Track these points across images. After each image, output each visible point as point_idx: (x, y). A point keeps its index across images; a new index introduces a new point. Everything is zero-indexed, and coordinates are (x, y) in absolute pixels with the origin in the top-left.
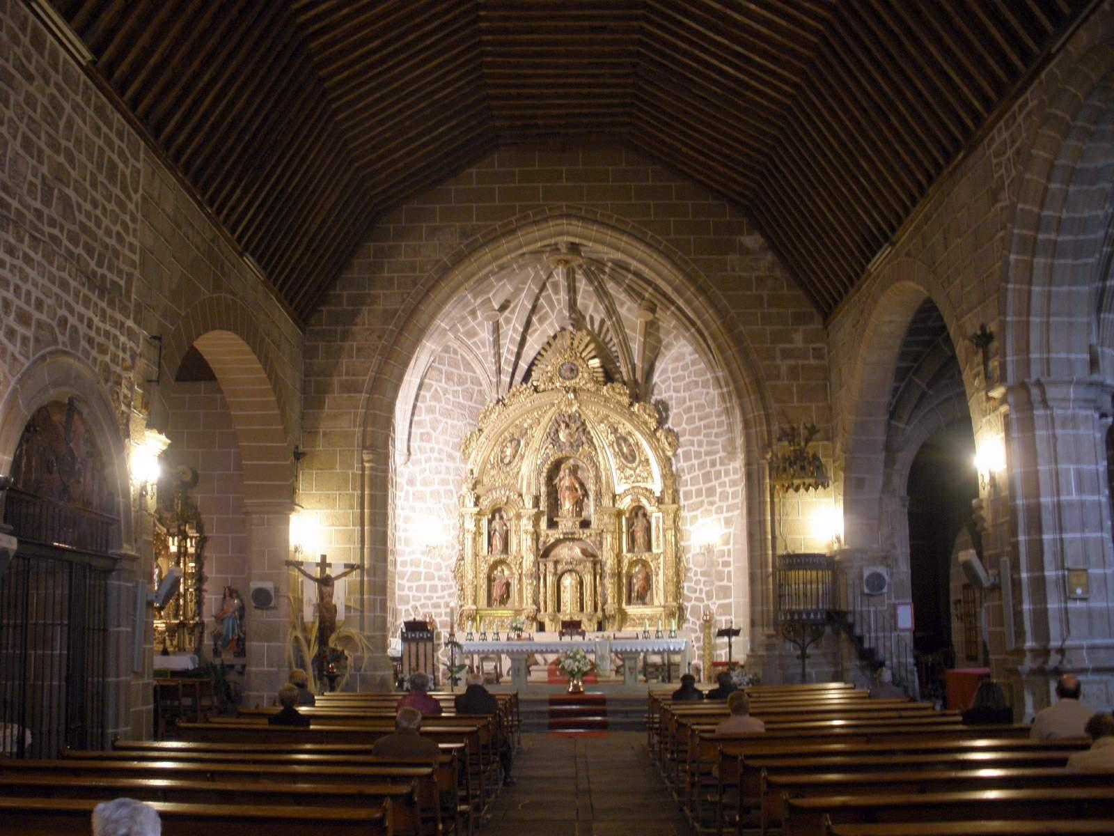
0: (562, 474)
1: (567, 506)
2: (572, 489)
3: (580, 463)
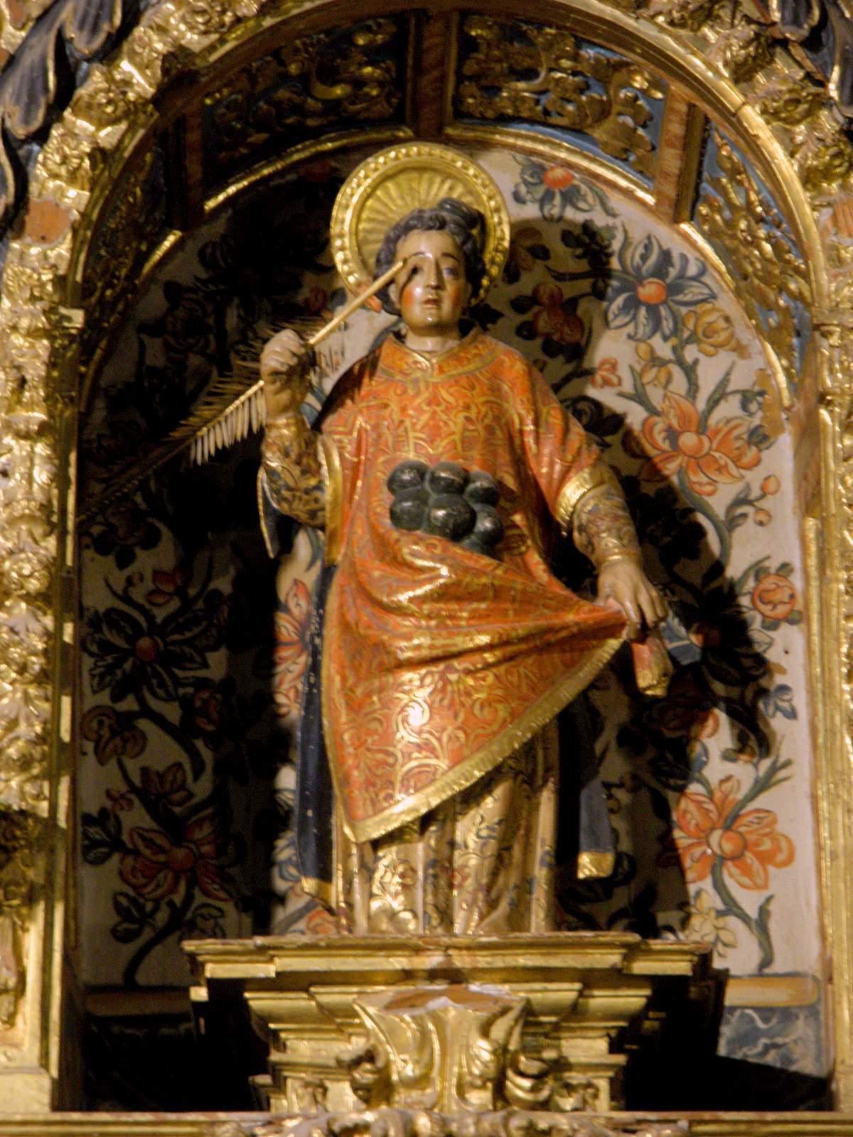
0: (345, 336)
1: (411, 727)
2: (489, 512)
3: (628, 208)
